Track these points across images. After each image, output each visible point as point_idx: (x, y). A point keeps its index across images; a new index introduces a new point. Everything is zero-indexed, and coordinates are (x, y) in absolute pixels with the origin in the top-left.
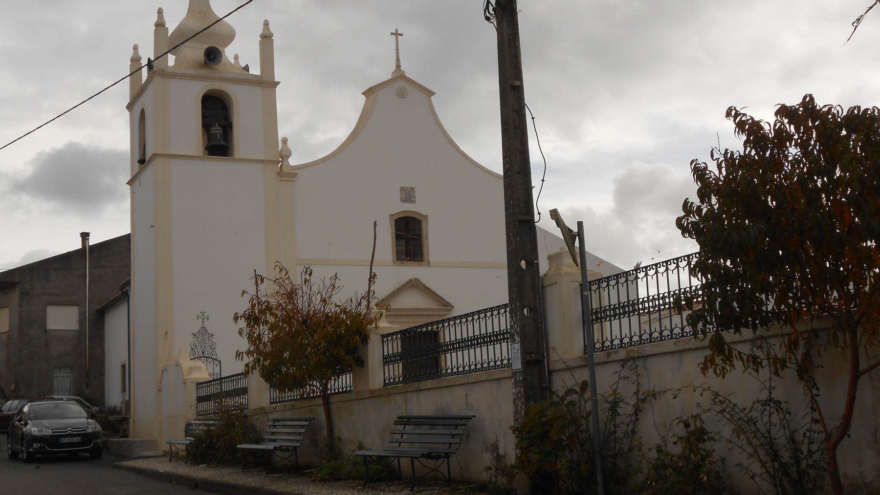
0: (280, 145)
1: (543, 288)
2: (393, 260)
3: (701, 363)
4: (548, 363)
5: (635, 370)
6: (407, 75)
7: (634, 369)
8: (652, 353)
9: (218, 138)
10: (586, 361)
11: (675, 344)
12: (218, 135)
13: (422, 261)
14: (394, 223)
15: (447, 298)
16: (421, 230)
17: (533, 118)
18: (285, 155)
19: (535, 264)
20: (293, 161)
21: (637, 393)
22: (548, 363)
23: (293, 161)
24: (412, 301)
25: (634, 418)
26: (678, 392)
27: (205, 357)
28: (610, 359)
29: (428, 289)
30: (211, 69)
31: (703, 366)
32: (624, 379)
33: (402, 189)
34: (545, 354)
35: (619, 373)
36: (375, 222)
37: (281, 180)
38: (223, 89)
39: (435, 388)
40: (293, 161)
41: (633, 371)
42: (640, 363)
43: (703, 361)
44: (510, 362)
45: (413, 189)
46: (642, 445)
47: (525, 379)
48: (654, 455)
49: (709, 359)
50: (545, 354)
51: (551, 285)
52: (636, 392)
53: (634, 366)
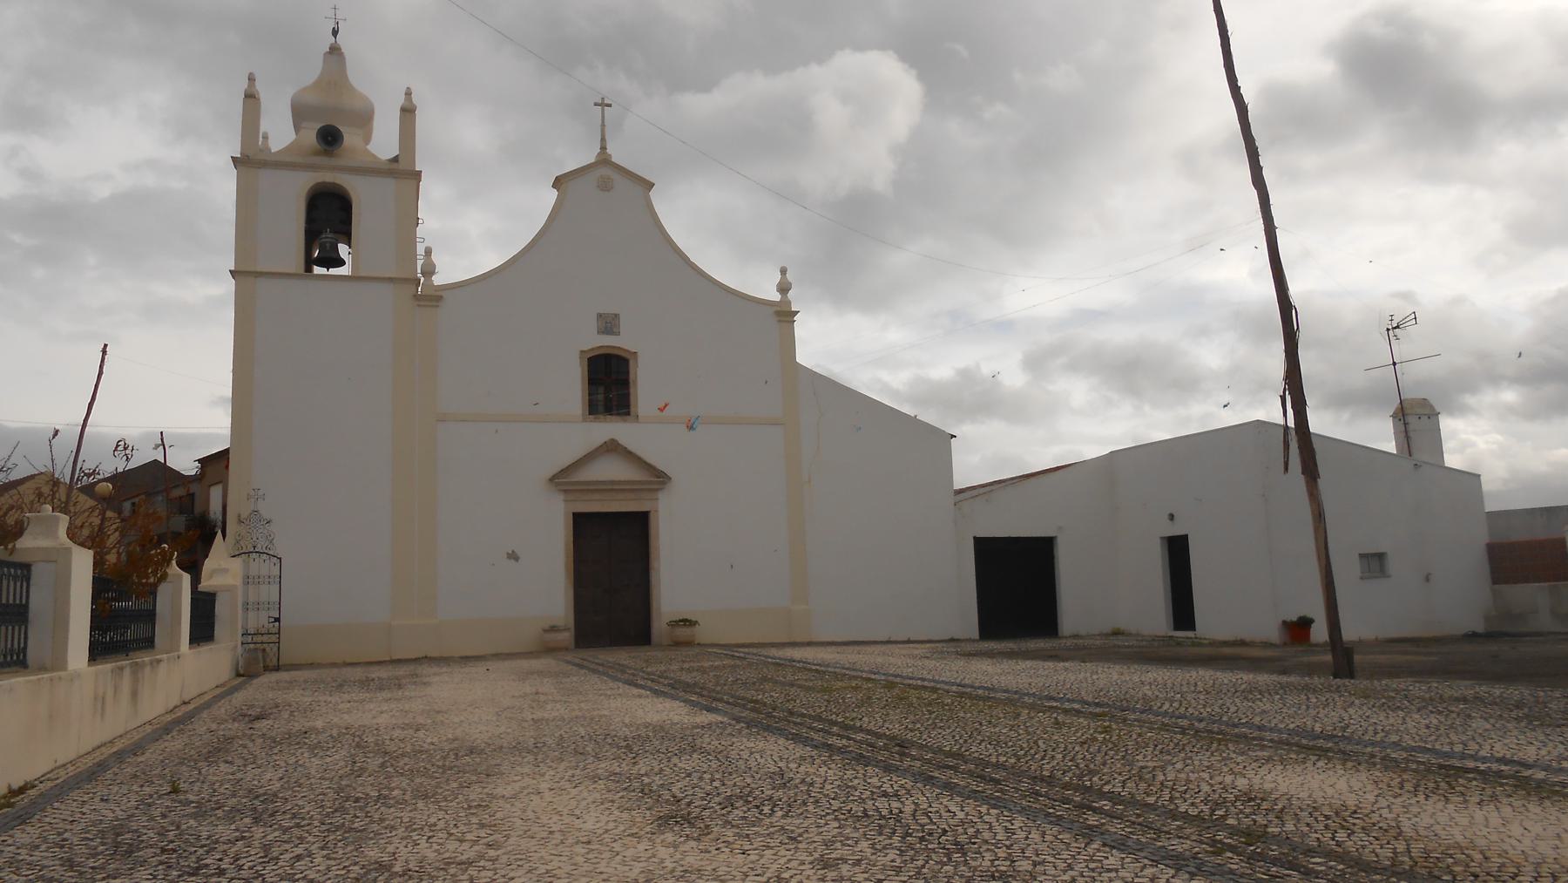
2: (583, 415)
9: (328, 248)
12: (328, 245)
13: (628, 414)
14: (586, 363)
15: (661, 466)
16: (628, 373)
20: (438, 280)
24: (609, 470)
27: (256, 552)
29: (630, 453)
33: (600, 316)
36: (106, 346)
37: (419, 306)
38: (338, 182)
45: (616, 316)
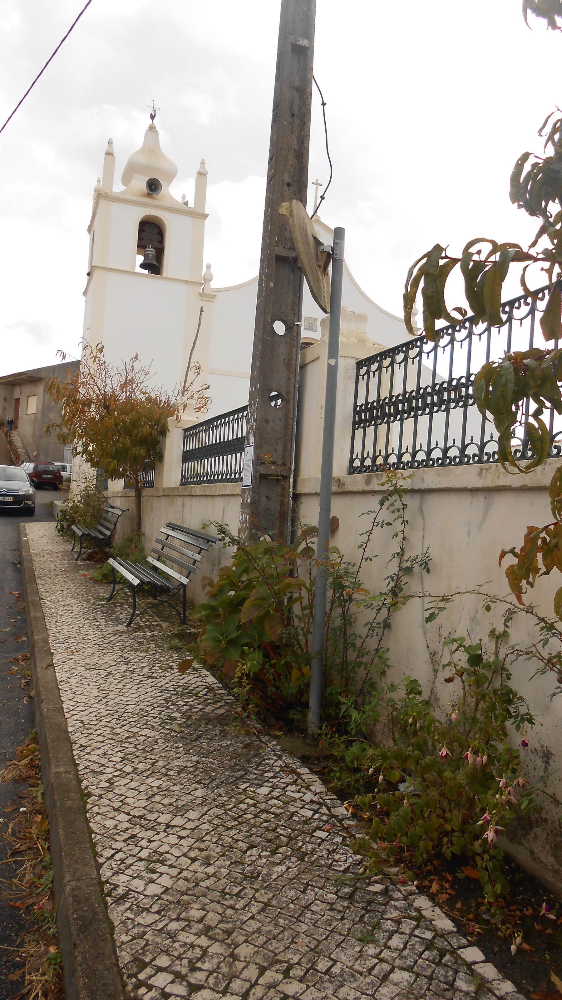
0: (204, 270)
1: (303, 367)
3: (512, 551)
4: (295, 481)
5: (402, 511)
6: (322, 220)
7: (398, 510)
8: (433, 486)
10: (338, 487)
11: (480, 474)
12: (151, 255)
17: (324, 104)
18: (208, 279)
19: (296, 327)
21: (401, 554)
22: (295, 481)
23: (215, 284)
25: (389, 600)
26: (442, 604)
28: (368, 488)
30: (153, 198)
31: (515, 561)
32: (382, 527)
34: (293, 468)
35: (374, 515)
36: (202, 308)
39: (202, 495)
40: (215, 284)
41: (397, 514)
42: (412, 502)
43: (519, 544)
44: (241, 476)
46: (388, 666)
47: (253, 502)
48: (400, 694)
49: (544, 540)
50: (293, 468)
51: (314, 361)
52: (398, 554)
53: (398, 505)
